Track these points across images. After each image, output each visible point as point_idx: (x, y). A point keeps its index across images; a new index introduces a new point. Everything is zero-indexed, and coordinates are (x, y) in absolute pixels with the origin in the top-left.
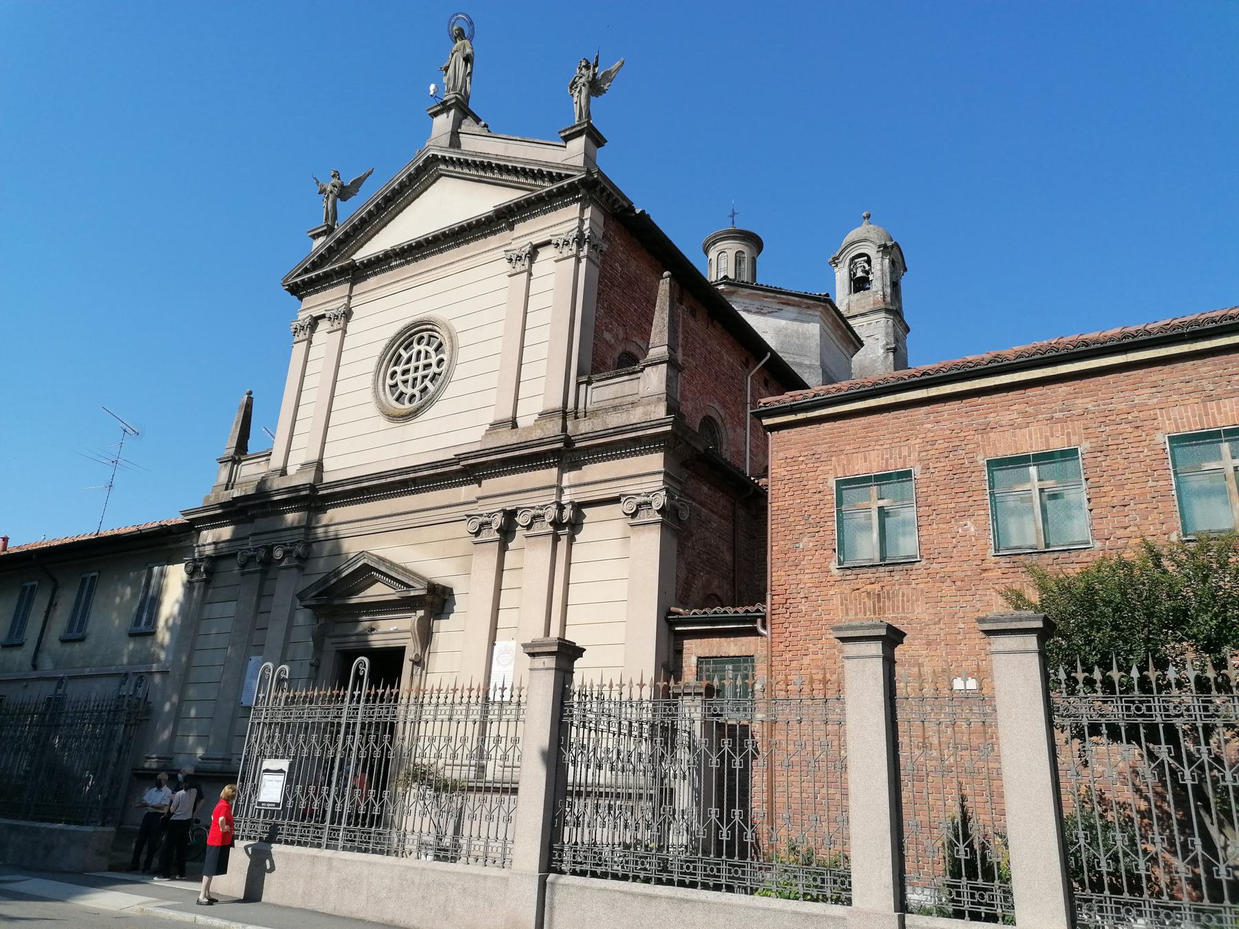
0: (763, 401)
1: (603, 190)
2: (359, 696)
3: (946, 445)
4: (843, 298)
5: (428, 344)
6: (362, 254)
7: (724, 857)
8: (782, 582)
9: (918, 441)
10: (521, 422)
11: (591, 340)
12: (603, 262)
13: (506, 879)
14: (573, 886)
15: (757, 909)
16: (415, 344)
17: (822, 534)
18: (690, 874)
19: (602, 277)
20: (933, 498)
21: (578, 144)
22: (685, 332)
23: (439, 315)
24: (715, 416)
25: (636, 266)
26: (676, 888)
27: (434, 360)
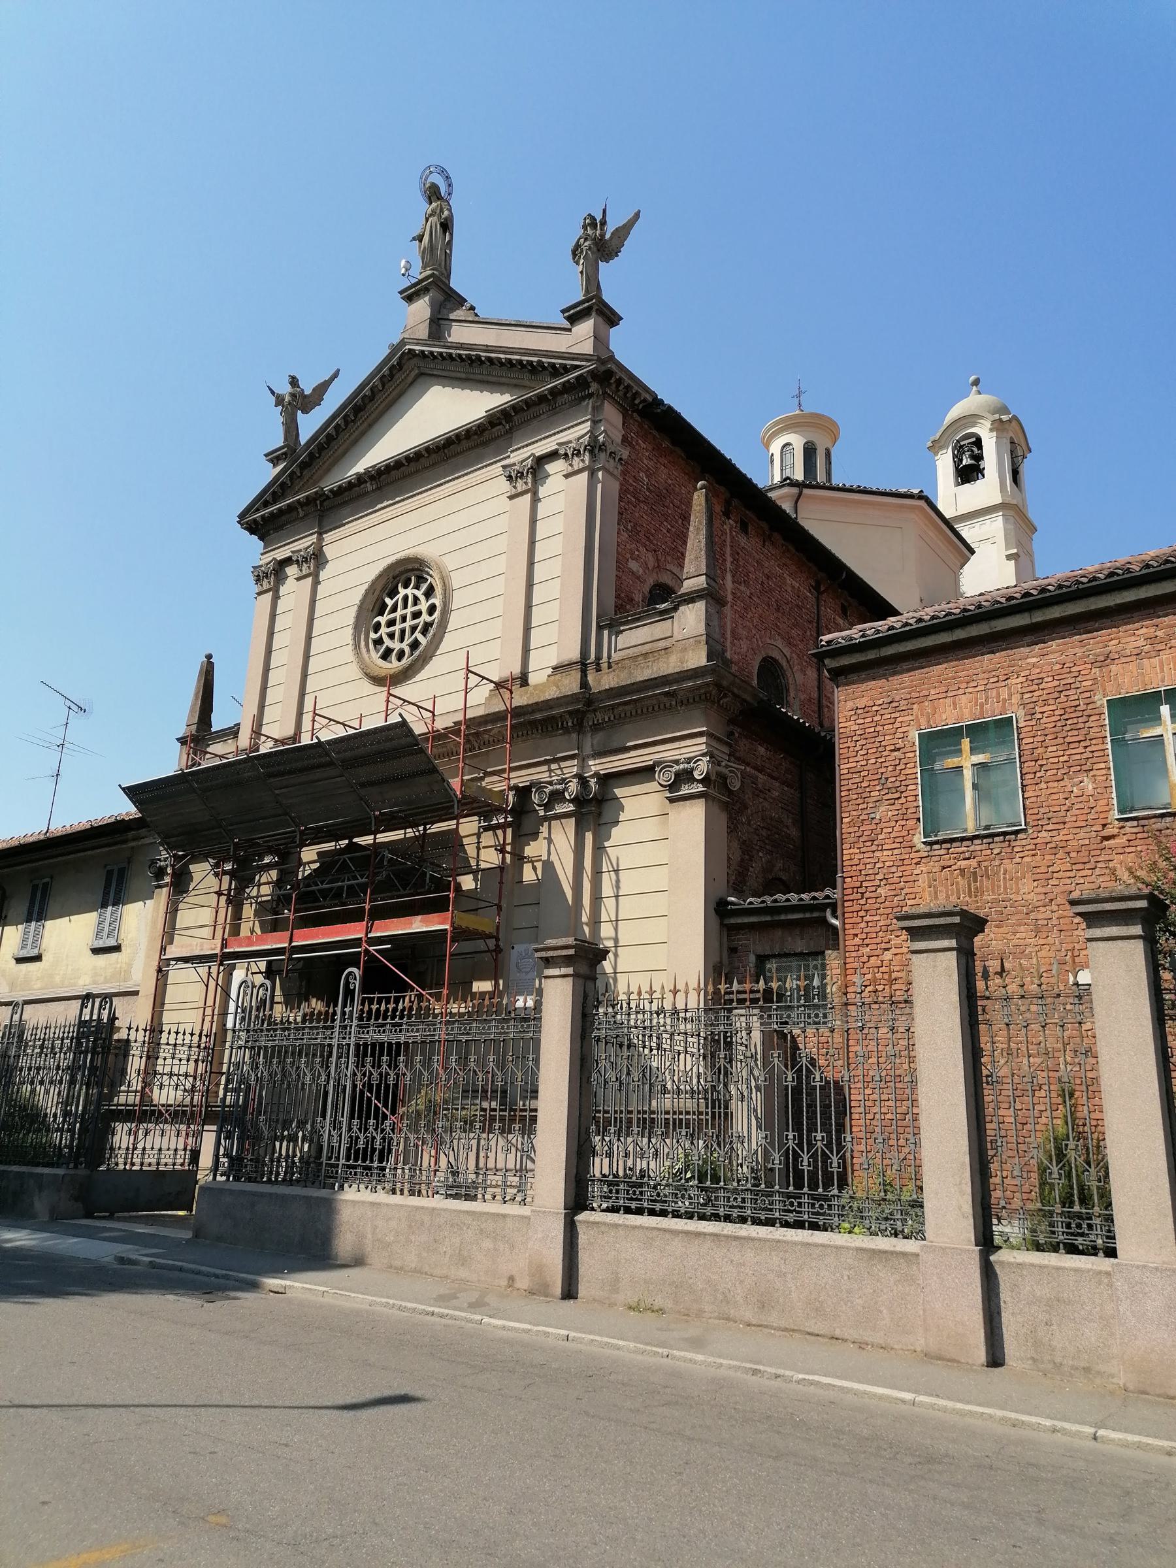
0: (826, 638)
1: (619, 381)
2: (351, 1012)
3: (1056, 683)
4: (952, 498)
5: (417, 587)
6: (330, 483)
7: (806, 1190)
8: (856, 862)
9: (1021, 679)
10: (533, 679)
11: (613, 573)
12: (624, 473)
13: (528, 1218)
14: (605, 1224)
15: (816, 1245)
16: (400, 588)
17: (903, 800)
18: (637, 1200)
19: (623, 492)
20: (1040, 750)
21: (586, 328)
22: (735, 554)
23: (426, 551)
24: (778, 657)
25: (667, 474)
26: (723, 1224)
27: (424, 606)
